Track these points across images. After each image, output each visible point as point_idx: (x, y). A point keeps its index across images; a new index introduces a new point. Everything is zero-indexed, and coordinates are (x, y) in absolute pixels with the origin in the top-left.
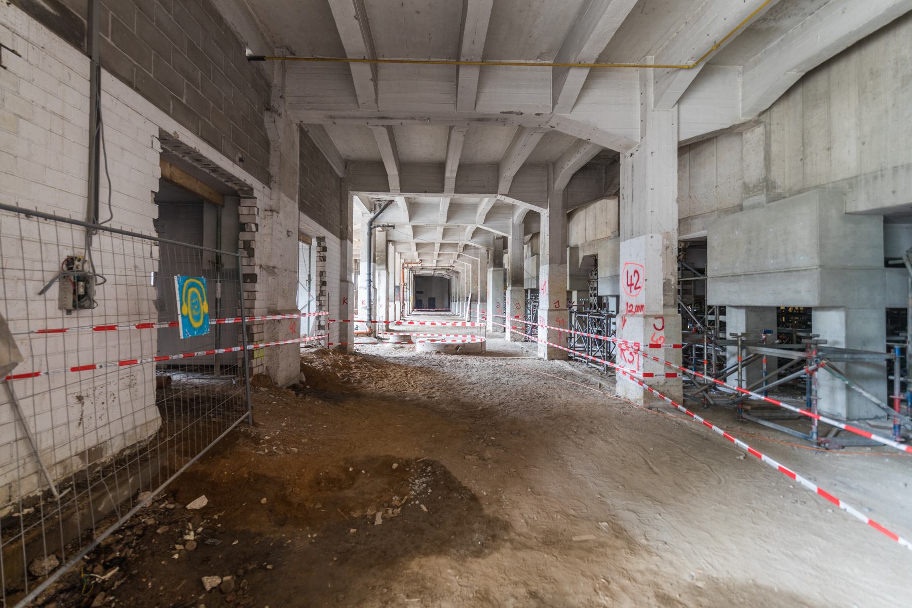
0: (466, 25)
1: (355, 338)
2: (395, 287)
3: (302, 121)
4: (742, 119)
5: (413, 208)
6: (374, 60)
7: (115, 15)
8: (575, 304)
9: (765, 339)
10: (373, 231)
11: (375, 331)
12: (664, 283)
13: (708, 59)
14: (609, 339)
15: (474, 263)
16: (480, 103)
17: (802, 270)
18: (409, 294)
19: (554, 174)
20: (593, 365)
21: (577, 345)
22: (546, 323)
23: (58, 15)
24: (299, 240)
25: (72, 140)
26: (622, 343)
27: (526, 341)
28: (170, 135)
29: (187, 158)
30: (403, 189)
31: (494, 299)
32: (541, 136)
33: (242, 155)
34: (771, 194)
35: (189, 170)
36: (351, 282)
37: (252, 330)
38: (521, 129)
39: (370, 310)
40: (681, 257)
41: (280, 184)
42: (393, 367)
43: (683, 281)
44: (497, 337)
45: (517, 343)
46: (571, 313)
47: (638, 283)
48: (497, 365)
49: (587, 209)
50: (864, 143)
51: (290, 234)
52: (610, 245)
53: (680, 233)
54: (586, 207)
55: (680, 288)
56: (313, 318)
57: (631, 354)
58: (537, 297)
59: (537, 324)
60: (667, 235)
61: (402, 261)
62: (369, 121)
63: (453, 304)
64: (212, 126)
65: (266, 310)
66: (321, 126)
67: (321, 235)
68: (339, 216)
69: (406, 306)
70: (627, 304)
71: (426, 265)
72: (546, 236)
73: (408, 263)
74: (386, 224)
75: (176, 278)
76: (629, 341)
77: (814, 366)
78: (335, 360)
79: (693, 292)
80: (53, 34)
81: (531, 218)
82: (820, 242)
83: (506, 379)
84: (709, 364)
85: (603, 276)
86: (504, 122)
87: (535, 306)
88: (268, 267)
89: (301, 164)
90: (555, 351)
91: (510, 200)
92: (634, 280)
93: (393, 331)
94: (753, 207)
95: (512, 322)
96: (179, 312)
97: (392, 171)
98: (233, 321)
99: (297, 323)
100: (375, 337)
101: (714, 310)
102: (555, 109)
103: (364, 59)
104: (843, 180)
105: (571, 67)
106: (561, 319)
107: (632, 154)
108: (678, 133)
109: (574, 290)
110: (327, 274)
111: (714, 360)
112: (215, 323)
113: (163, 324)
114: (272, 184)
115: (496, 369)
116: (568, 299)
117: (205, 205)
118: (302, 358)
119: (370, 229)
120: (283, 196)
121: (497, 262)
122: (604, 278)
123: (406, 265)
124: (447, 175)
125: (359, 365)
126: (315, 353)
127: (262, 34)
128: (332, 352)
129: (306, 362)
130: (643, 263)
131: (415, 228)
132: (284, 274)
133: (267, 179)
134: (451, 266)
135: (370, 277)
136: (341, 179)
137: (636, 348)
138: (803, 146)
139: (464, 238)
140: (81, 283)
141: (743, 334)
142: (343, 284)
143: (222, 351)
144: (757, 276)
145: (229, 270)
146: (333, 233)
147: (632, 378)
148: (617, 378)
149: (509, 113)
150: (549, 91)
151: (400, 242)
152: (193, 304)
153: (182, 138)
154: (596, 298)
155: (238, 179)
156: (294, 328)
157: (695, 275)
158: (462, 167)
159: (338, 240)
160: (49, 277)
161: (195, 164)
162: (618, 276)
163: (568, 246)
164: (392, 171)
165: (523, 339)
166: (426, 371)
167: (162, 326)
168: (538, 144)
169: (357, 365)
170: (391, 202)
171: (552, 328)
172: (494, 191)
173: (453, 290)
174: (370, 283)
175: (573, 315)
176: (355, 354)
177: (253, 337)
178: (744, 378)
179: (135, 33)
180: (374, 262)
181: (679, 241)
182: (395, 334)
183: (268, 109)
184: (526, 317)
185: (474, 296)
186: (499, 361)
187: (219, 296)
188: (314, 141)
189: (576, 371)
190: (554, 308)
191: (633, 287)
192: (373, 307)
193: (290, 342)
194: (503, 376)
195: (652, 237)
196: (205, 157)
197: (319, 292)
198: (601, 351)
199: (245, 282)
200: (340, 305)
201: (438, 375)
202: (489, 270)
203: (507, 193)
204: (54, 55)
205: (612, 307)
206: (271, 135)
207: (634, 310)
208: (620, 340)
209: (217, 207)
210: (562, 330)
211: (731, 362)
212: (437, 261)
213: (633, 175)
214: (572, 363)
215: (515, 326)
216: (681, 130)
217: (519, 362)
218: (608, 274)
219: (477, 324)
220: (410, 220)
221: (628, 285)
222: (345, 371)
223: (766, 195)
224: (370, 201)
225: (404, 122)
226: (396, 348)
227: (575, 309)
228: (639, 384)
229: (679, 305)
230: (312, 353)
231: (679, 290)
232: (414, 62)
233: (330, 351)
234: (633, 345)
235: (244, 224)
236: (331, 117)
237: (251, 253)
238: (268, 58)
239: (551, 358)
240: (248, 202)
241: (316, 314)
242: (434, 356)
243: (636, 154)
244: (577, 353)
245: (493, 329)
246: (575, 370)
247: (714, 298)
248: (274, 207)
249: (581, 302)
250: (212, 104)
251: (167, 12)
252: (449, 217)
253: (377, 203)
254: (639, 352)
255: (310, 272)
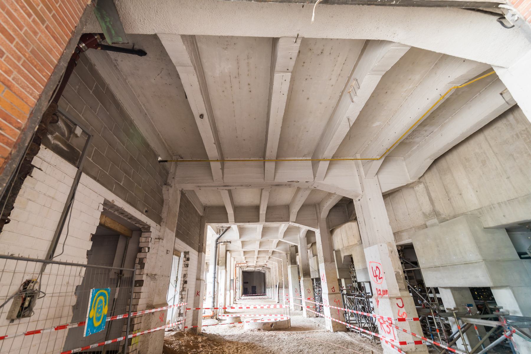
0: (269, 136)
1: (203, 321)
2: (231, 280)
3: (183, 189)
4: (411, 181)
5: (242, 231)
6: (222, 160)
7: (97, 149)
8: (345, 288)
9: (470, 310)
10: (218, 245)
11: (217, 314)
12: (396, 274)
13: (386, 155)
14: (371, 315)
15: (279, 262)
16: (276, 177)
17: (474, 263)
18: (239, 284)
19: (320, 210)
20: (365, 335)
21: (351, 318)
22: (328, 304)
23: (68, 151)
24: (173, 254)
25: (54, 210)
26: (380, 318)
27: (317, 317)
28: (110, 202)
29: (116, 213)
30: (236, 221)
31: (293, 286)
32: (310, 191)
33: (147, 209)
34: (440, 218)
35: (115, 219)
36: (203, 280)
37: (134, 322)
38: (299, 189)
39: (214, 298)
40: (401, 255)
41: (166, 223)
42: (228, 344)
43: (407, 271)
44: (297, 314)
45: (312, 319)
46: (343, 295)
47: (380, 275)
48: (299, 338)
49: (341, 228)
50: (477, 191)
51: (168, 252)
52: (358, 249)
53: (396, 240)
54: (340, 227)
55: (406, 275)
56: (176, 308)
57: (387, 326)
58: (320, 284)
59: (322, 305)
60: (389, 244)
61: (235, 262)
62: (219, 188)
63: (267, 290)
64: (134, 195)
65: (145, 306)
66: (193, 191)
67: (187, 251)
68: (198, 238)
69: (237, 293)
70: (377, 289)
71: (249, 264)
72: (320, 245)
73: (239, 264)
74: (226, 241)
75: (91, 290)
76: (384, 317)
77: (508, 333)
78: (188, 341)
79: (414, 277)
80: (63, 159)
81: (310, 235)
82: (477, 245)
83: (307, 350)
84: (440, 331)
85: (358, 269)
86: (290, 186)
87: (319, 290)
88: (152, 275)
89: (180, 210)
90: (337, 324)
91: (297, 225)
92: (378, 273)
93: (229, 313)
94: (433, 225)
95: (306, 302)
96: (87, 316)
97: (230, 211)
98: (122, 317)
99: (165, 314)
100: (217, 319)
101: (431, 289)
102: (315, 179)
103: (218, 160)
104: (475, 210)
105: (320, 160)
106: (338, 300)
107: (359, 200)
108: (381, 188)
109: (342, 278)
110: (188, 276)
111: (443, 328)
112: (109, 320)
113: (74, 325)
114: (162, 223)
115: (299, 341)
116: (339, 285)
117: (121, 236)
118: (165, 341)
119: (217, 244)
120: (167, 229)
121: (293, 261)
122: (359, 270)
123: (237, 265)
124: (261, 212)
125: (205, 344)
126: (175, 336)
127: (168, 151)
128: (187, 335)
129: (167, 344)
130: (380, 262)
131: (243, 242)
132: (161, 279)
133: (159, 220)
134: (265, 265)
135: (215, 275)
136: (201, 216)
137: (390, 322)
138: (447, 193)
139: (272, 247)
140: (29, 299)
141: (455, 309)
142: (198, 281)
143: (110, 342)
144: (449, 267)
145: (127, 278)
146: (194, 248)
147: (393, 346)
148: (383, 347)
149: (292, 181)
150: (311, 171)
151: (234, 251)
152: (98, 308)
153: (116, 203)
154: (356, 283)
155: (143, 222)
156: (163, 315)
157: (413, 267)
158: (269, 208)
159: (197, 253)
160: (10, 294)
161: (120, 215)
162: (367, 268)
163: (334, 250)
164: (230, 211)
165: (315, 316)
166: (251, 346)
167: (74, 326)
168: (309, 195)
169: (202, 344)
170: (229, 227)
171: (333, 307)
172: (287, 220)
173: (267, 280)
174: (215, 279)
175: (345, 296)
176: (202, 335)
177: (133, 327)
178: (467, 342)
179: (104, 155)
180: (218, 265)
181: (397, 246)
182: (230, 315)
183: (165, 184)
184: (314, 299)
185: (280, 284)
186: (301, 334)
187: (116, 296)
188: (188, 197)
189: (354, 340)
190: (332, 292)
191: (378, 278)
192: (216, 296)
193: (158, 329)
194: (305, 347)
195: (381, 246)
196: (127, 212)
197: (182, 289)
198: (367, 323)
199: (135, 286)
200: (195, 297)
201: (259, 349)
202: (288, 267)
203: (295, 221)
204: (60, 168)
205: (368, 290)
206: (165, 197)
207: (382, 293)
208: (378, 316)
209: (127, 238)
210: (339, 308)
211: (454, 329)
212: (257, 262)
213: (362, 211)
214: (350, 333)
215: (309, 306)
216: (382, 187)
217: (315, 334)
218: (361, 268)
219: (284, 306)
220: (240, 238)
221: (375, 276)
222: (194, 350)
223: (437, 219)
224: (217, 228)
225: (237, 187)
226: (230, 327)
227: (345, 292)
228: (399, 351)
229: (409, 287)
230: (172, 336)
231: (406, 277)
232: (242, 160)
233: (185, 333)
234: (387, 319)
235: (142, 248)
236: (198, 186)
237: (142, 265)
238: (169, 161)
239: (335, 331)
240: (146, 234)
241: (178, 306)
242: (257, 333)
243: (361, 200)
244: (352, 326)
245: (294, 308)
246: (353, 340)
247: (429, 283)
248: (161, 237)
249: (348, 286)
250: (136, 184)
251: (123, 145)
252: (263, 235)
253: (221, 228)
254: (392, 325)
255: (177, 274)
